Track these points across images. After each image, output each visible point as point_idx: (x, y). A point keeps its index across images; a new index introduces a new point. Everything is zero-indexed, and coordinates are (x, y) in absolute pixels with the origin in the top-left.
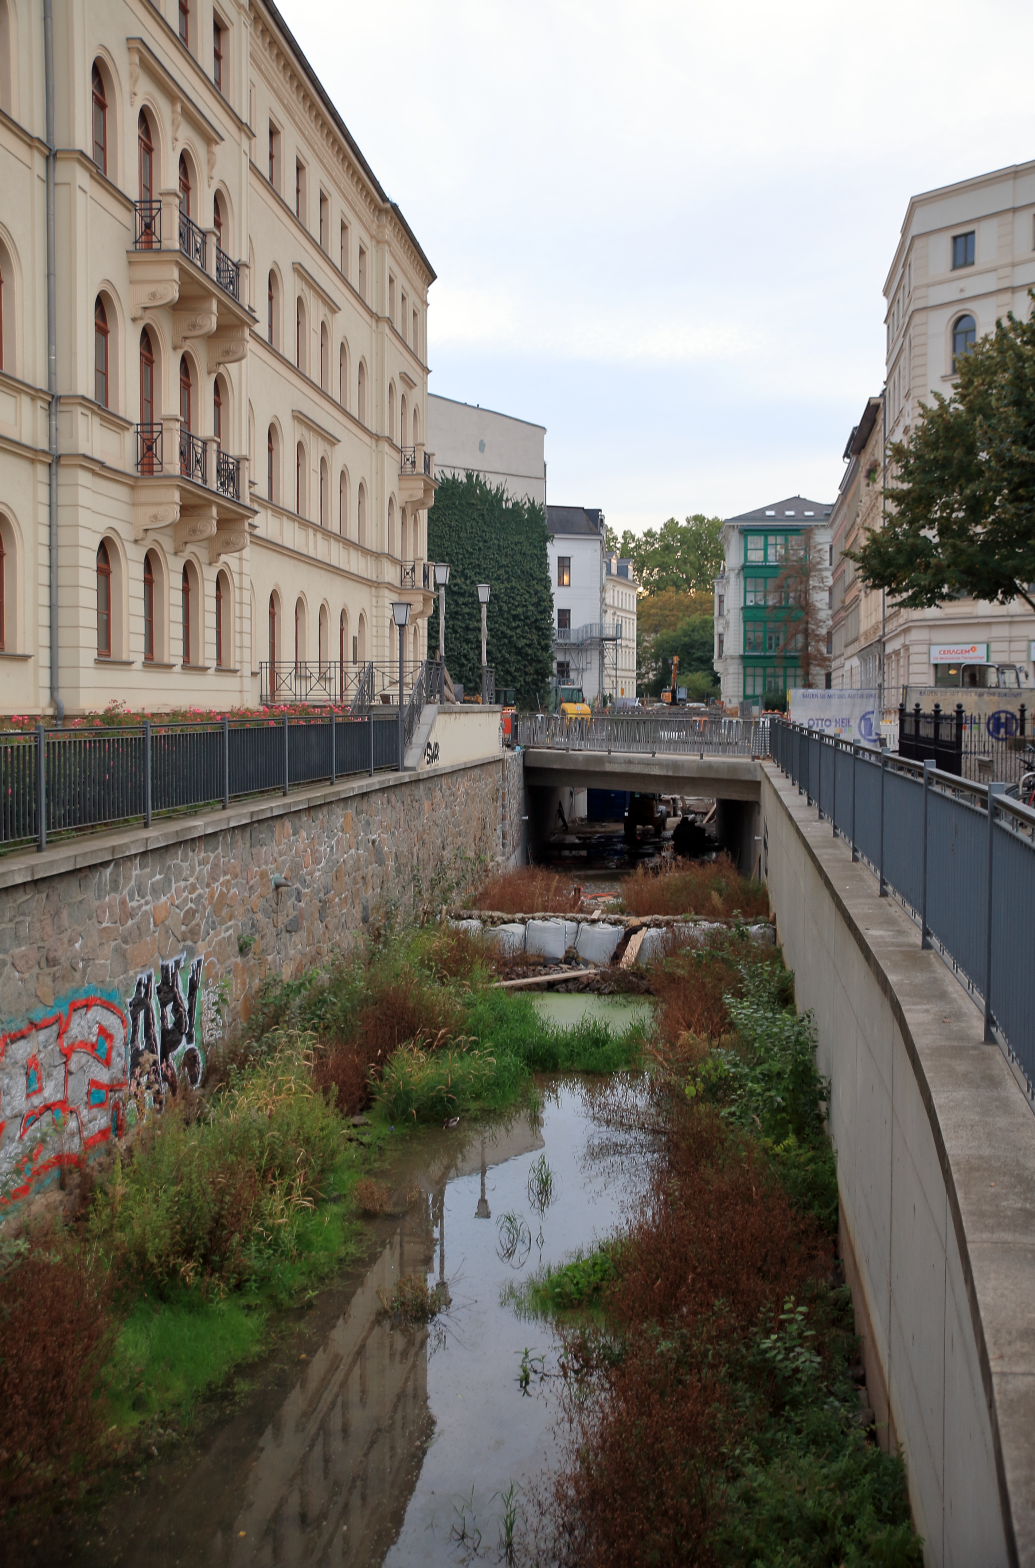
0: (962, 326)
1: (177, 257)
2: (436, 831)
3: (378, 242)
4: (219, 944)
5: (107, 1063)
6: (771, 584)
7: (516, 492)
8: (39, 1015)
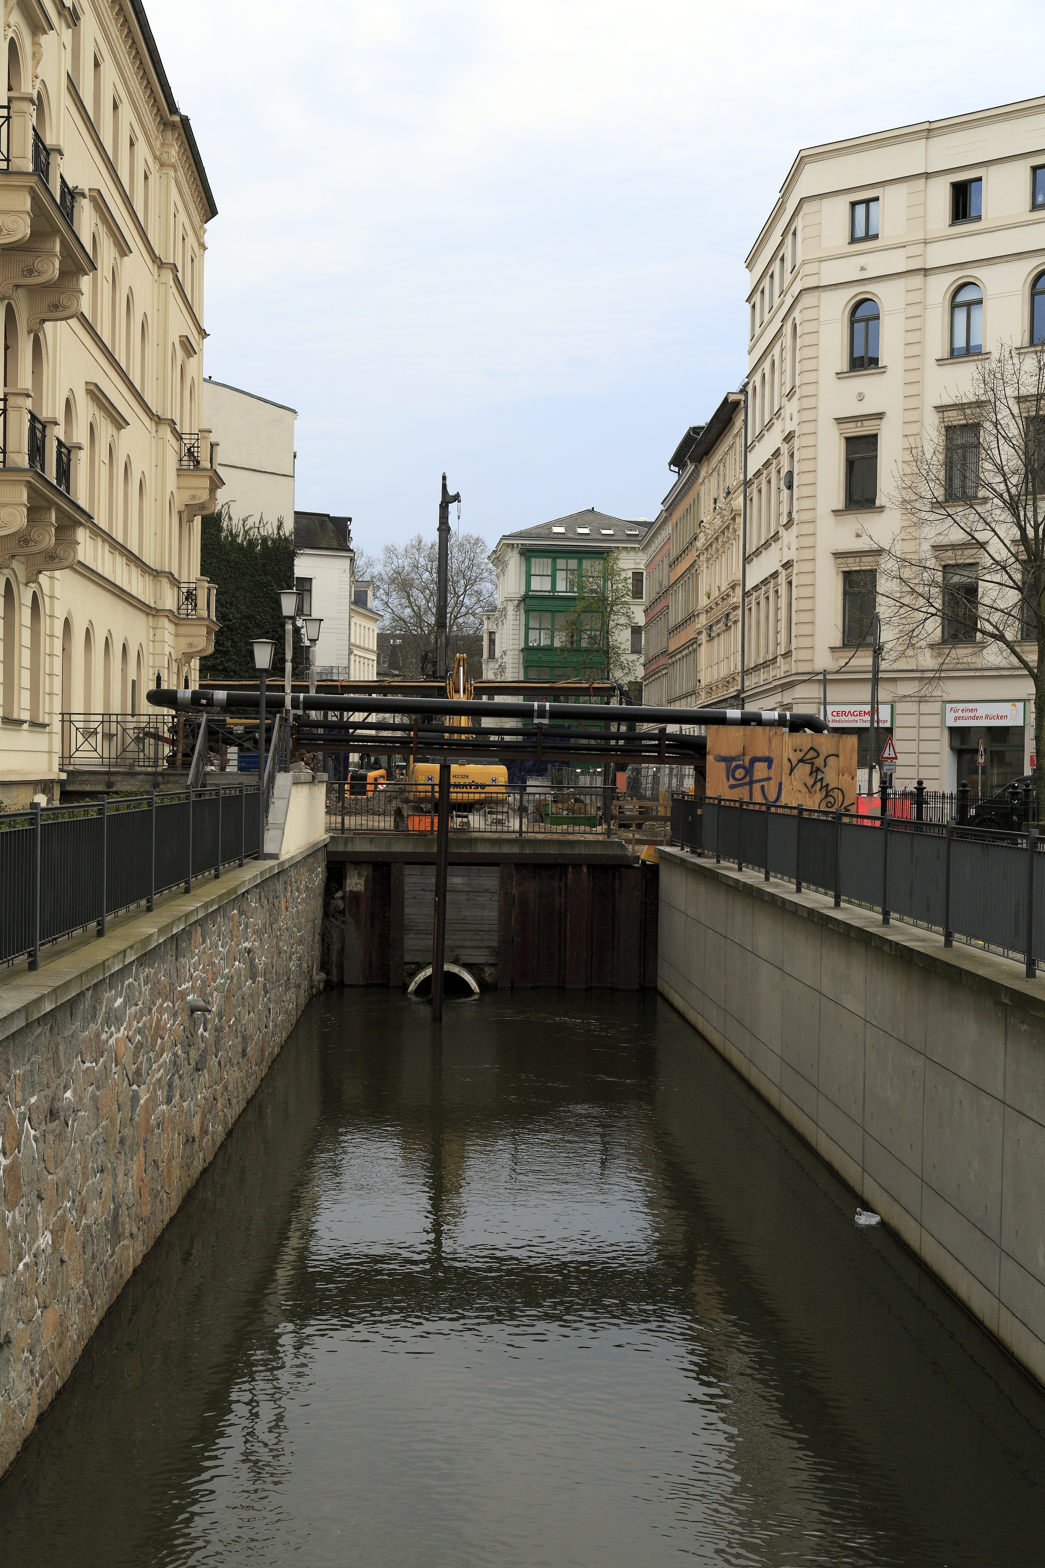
0: (861, 313)
1: (33, 181)
3: (162, 165)
6: (561, 620)
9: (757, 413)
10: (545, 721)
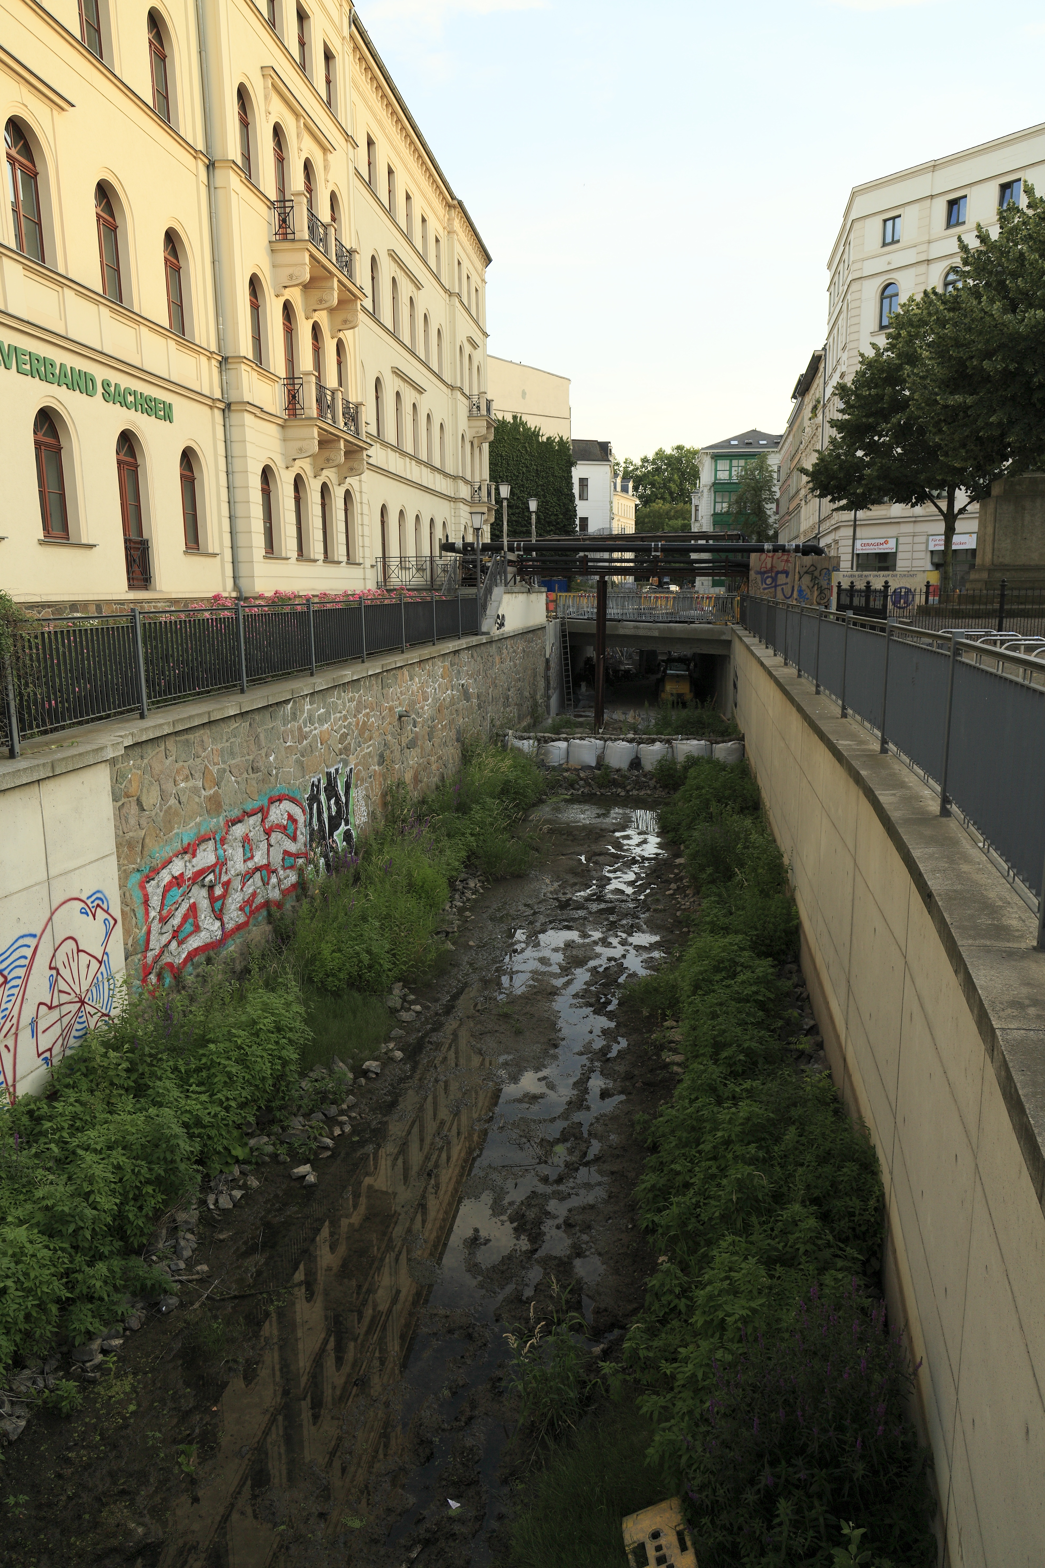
0: (888, 292)
2: (503, 677)
4: (364, 757)
5: (294, 839)
7: (549, 430)
8: (249, 806)
9: (830, 362)
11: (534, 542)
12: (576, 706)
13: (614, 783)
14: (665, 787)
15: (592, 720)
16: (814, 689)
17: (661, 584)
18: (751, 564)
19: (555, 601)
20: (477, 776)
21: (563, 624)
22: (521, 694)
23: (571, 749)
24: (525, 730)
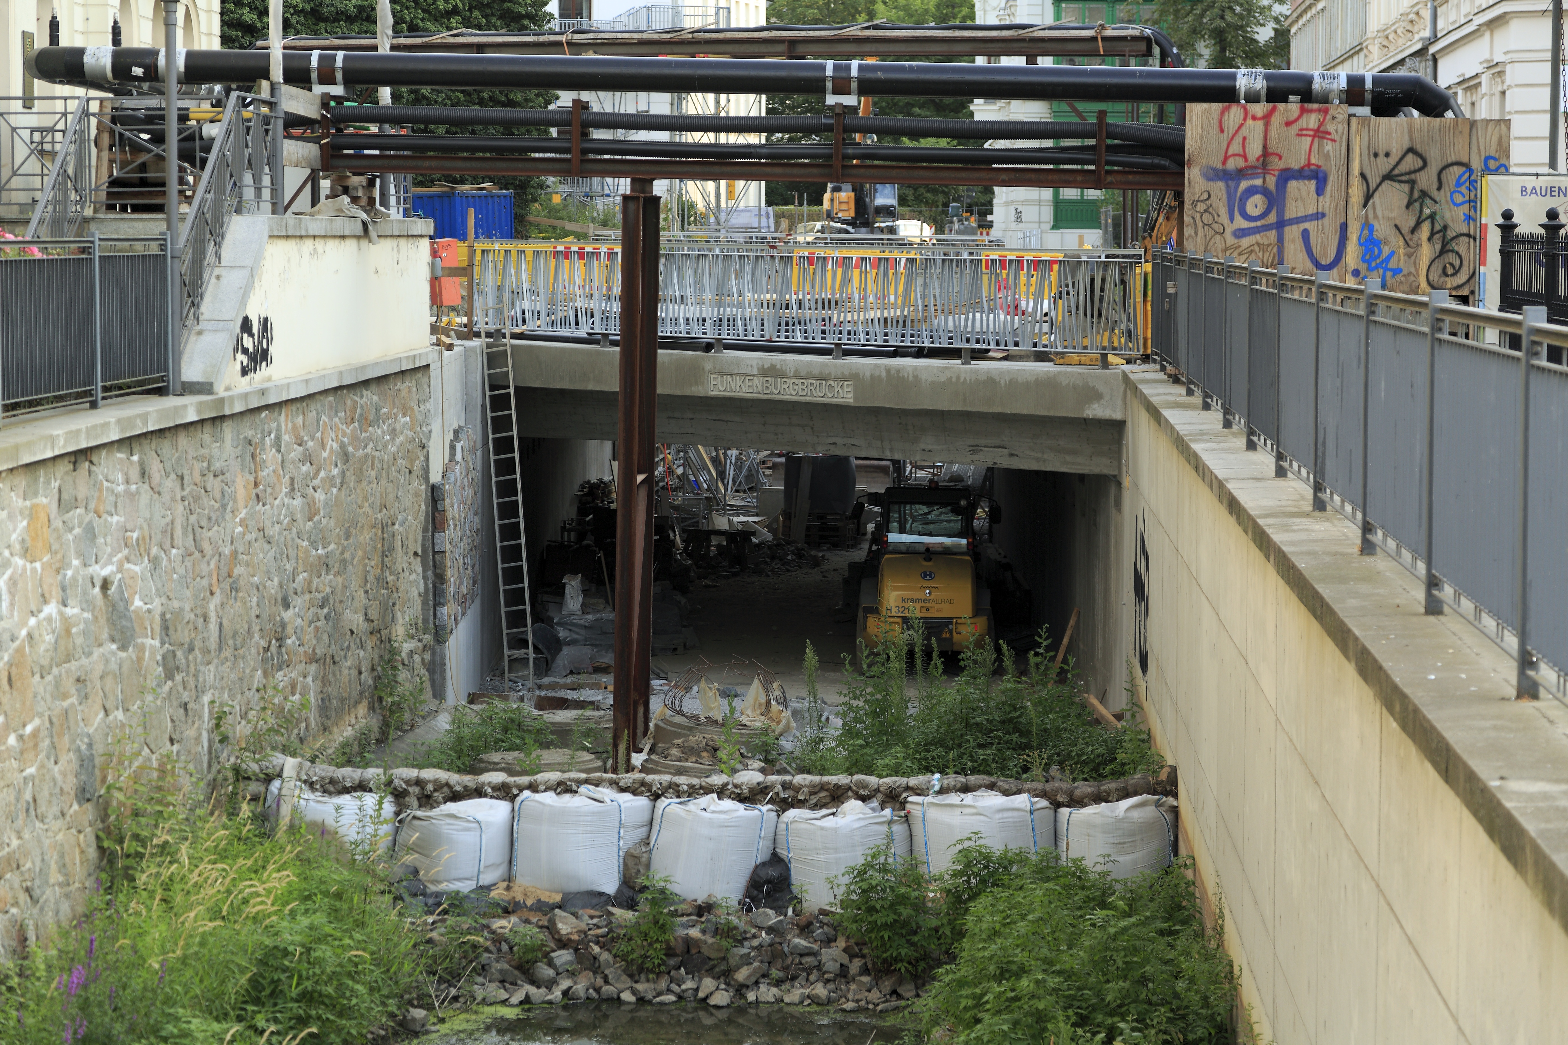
2: (264, 555)
10: (850, 100)
11: (384, 49)
12: (544, 667)
13: (690, 958)
14: (881, 969)
15: (603, 717)
16: (1419, 594)
17: (863, 216)
18: (1191, 145)
19: (466, 271)
20: (157, 933)
21: (493, 359)
22: (333, 618)
23: (523, 828)
24: (350, 756)
